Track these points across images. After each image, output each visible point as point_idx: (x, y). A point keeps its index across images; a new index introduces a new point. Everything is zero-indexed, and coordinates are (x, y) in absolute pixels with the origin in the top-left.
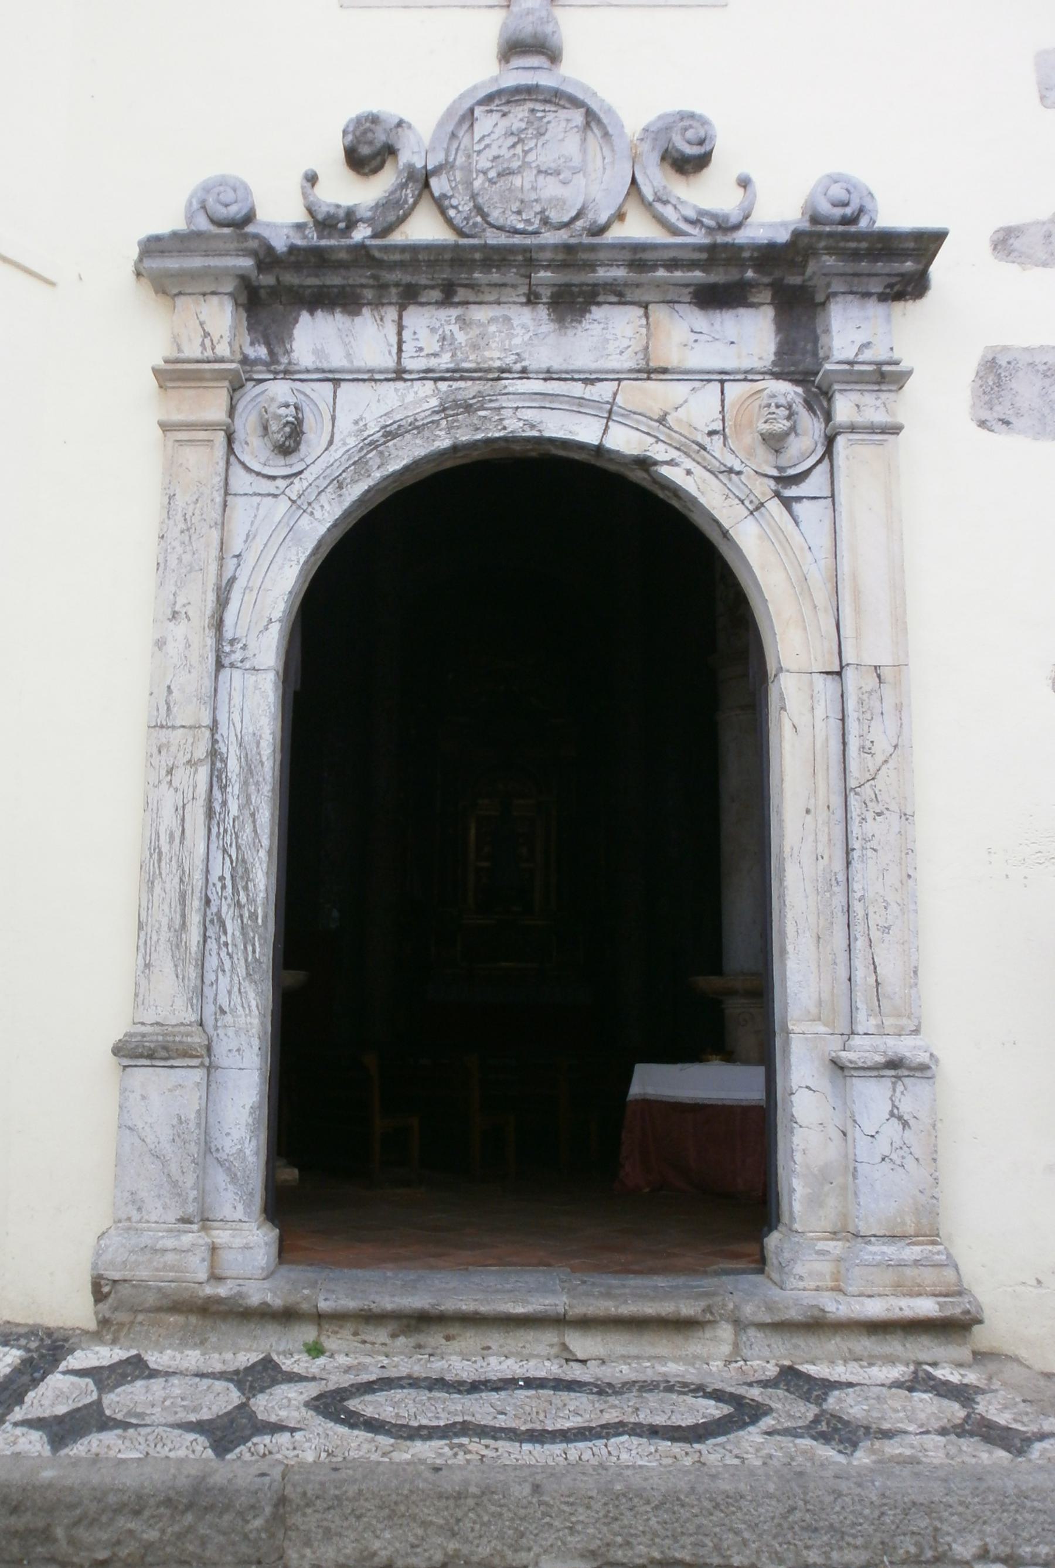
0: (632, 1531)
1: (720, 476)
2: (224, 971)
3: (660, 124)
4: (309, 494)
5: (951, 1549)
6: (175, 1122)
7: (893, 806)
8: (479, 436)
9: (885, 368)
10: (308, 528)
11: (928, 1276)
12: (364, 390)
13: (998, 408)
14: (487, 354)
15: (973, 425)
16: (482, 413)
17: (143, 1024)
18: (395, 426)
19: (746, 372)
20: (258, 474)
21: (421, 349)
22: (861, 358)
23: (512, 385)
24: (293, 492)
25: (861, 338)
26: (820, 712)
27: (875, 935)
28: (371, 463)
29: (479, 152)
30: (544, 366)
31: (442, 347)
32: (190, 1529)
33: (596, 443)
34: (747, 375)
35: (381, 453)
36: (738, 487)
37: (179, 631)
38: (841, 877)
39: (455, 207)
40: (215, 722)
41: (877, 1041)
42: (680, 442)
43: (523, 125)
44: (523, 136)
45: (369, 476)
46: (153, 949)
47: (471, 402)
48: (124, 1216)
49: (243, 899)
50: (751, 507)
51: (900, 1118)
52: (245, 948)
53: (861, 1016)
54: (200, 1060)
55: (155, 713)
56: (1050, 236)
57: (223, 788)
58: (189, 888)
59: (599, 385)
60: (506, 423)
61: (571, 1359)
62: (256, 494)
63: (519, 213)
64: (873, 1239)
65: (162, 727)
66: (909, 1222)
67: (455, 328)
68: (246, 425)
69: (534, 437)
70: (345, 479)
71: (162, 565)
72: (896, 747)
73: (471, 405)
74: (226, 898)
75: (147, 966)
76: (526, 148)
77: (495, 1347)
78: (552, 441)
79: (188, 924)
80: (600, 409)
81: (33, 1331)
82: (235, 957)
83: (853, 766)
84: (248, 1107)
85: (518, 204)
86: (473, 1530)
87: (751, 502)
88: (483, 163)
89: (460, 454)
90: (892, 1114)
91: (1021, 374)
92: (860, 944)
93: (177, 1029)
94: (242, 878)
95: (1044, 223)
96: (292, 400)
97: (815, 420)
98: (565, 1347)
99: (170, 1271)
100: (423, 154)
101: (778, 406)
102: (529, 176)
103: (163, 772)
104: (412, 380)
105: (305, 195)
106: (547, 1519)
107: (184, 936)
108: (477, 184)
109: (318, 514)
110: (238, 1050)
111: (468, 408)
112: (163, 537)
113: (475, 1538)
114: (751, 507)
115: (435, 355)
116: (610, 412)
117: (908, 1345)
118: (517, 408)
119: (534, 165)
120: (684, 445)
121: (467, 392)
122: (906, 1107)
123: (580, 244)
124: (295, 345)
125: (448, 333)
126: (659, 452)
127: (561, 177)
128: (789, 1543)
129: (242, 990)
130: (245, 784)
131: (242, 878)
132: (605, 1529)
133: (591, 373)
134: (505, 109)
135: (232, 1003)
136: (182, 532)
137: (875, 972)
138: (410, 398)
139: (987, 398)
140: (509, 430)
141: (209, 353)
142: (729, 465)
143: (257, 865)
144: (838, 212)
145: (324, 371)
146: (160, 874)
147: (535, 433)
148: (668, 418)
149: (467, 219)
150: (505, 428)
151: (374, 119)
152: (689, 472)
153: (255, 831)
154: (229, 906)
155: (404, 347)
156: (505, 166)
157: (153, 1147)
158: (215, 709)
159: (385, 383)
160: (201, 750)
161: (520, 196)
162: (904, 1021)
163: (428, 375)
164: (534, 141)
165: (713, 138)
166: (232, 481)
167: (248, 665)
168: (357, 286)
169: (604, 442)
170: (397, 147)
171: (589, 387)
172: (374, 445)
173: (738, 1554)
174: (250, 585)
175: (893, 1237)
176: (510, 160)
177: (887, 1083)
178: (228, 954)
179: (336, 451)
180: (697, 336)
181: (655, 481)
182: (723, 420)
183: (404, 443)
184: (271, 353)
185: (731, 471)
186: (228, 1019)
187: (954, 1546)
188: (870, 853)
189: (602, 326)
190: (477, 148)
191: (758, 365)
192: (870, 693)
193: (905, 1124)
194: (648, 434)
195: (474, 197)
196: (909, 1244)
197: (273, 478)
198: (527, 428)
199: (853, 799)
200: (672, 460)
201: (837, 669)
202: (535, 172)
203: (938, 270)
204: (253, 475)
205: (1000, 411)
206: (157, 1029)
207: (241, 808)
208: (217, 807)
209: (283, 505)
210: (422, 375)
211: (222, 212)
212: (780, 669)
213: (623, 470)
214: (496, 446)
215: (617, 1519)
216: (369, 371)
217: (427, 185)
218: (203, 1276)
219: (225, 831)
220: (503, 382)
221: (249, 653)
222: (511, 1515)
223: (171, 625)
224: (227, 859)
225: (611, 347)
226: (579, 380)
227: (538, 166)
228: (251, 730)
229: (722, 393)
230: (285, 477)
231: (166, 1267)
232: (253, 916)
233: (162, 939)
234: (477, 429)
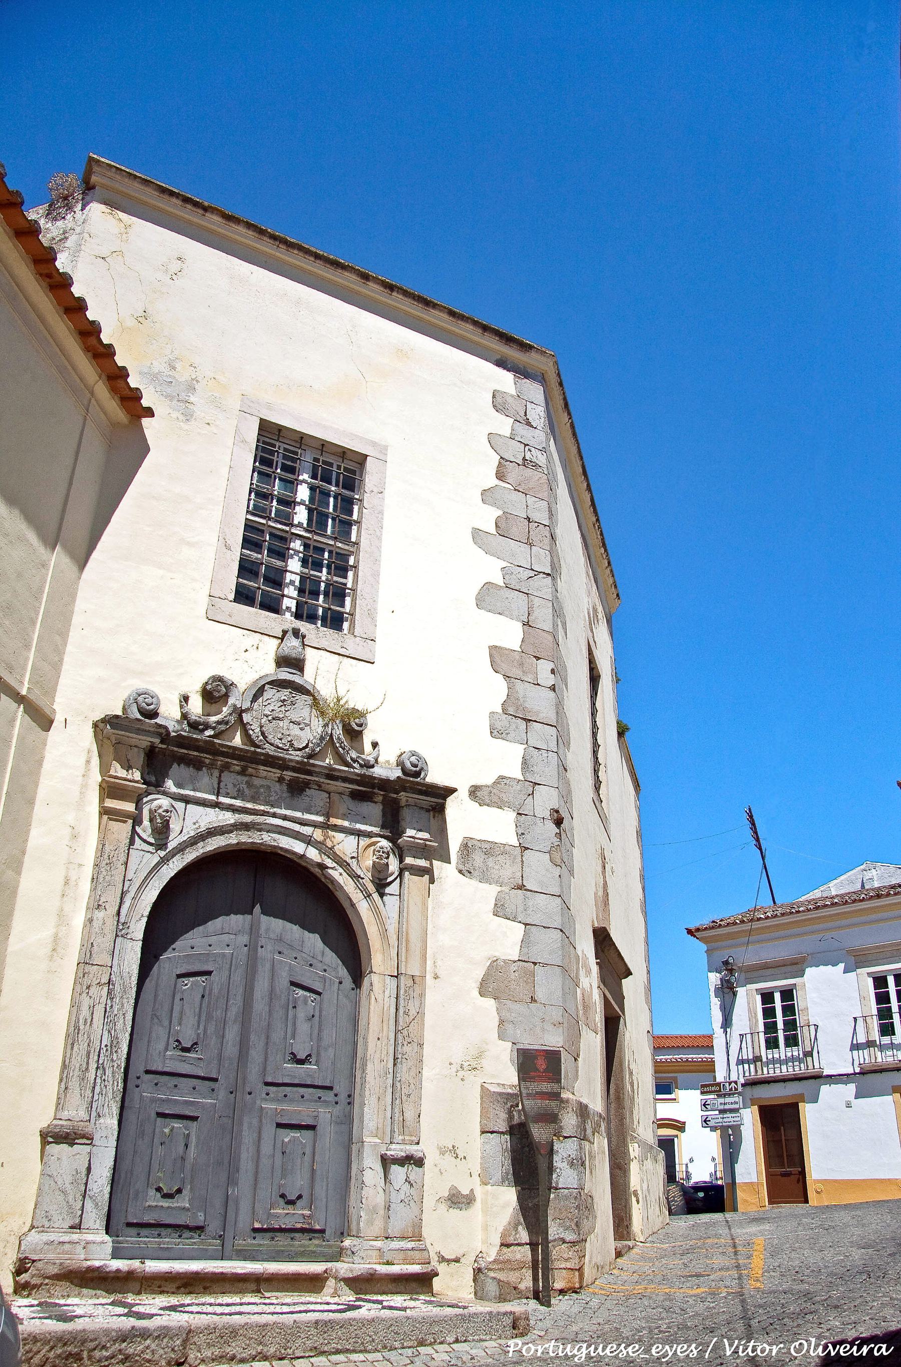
6: (74, 1173)
8: (250, 840)
12: (200, 809)
13: (466, 865)
21: (228, 794)
26: (387, 993)
32: (148, 1347)
38: (391, 1071)
39: (253, 730)
41: (402, 1147)
49: (115, 1058)
51: (410, 1182)
52: (113, 1083)
53: (396, 1135)
63: (281, 739)
78: (281, 848)
83: (401, 1020)
84: (108, 1167)
90: (406, 1180)
102: (286, 722)
105: (181, 707)
106: (299, 1334)
122: (411, 1178)
136: (107, 864)
138: (221, 817)
146: (78, 1040)
150: (262, 839)
152: (341, 874)
161: (282, 732)
162: (413, 1138)
165: (366, 725)
175: (403, 1238)
180: (350, 812)
185: (359, 877)
188: (404, 1060)
198: (272, 841)
199: (400, 1036)
206: (69, 1123)
212: (371, 972)
213: (309, 866)
221: (130, 931)
223: (96, 912)
228: (127, 970)
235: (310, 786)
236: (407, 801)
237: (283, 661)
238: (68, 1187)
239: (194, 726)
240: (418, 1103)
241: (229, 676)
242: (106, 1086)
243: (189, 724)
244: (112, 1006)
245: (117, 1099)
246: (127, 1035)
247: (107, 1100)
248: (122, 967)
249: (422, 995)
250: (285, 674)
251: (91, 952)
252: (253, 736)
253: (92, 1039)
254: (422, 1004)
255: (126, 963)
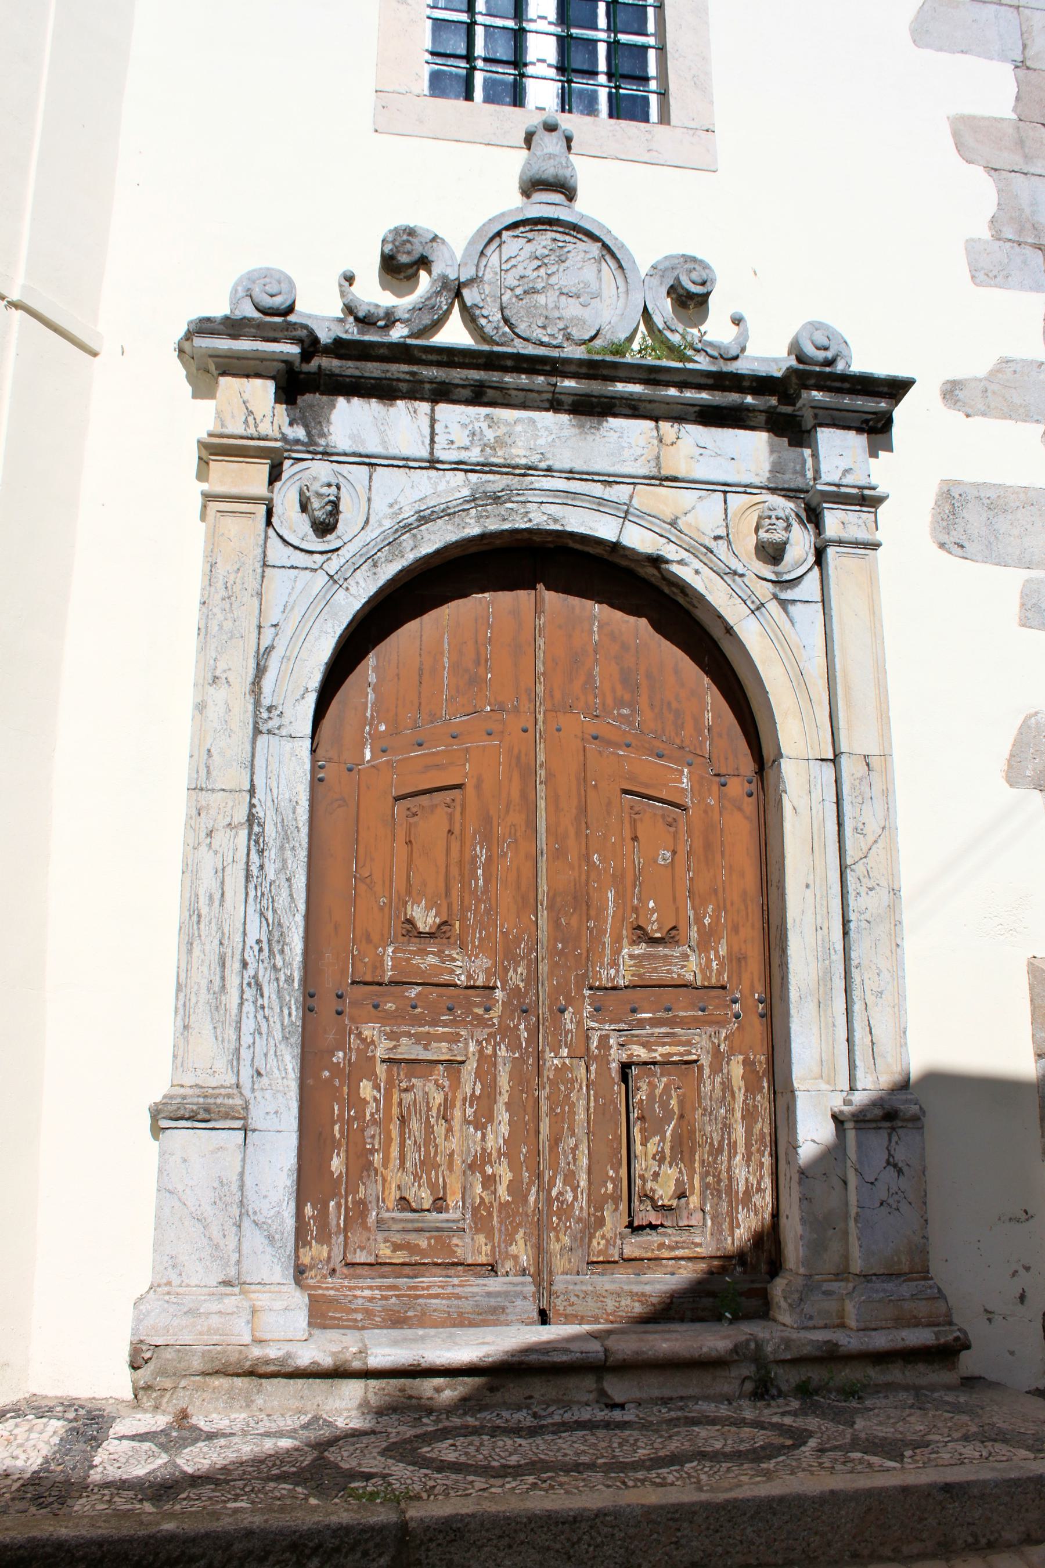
0: (731, 1541)
1: (725, 577)
2: (260, 1033)
3: (667, 264)
4: (346, 571)
5: (1000, 1536)
6: (216, 1184)
7: (884, 883)
8: (506, 526)
9: (867, 492)
10: (343, 603)
11: (922, 1309)
13: (953, 533)
14: (514, 451)
15: (935, 547)
16: (509, 505)
17: (182, 1086)
18: (429, 511)
19: (746, 486)
20: (296, 548)
21: (452, 442)
22: (844, 481)
23: (539, 482)
24: (333, 566)
25: (844, 464)
26: (816, 795)
27: (870, 999)
28: (404, 544)
29: (507, 271)
30: (567, 466)
31: (471, 442)
33: (614, 540)
34: (746, 488)
35: (414, 536)
36: (740, 587)
37: (218, 695)
38: (839, 946)
40: (253, 786)
42: (689, 544)
43: (546, 252)
44: (546, 261)
45: (403, 556)
46: (192, 1011)
47: (500, 494)
48: (164, 1281)
49: (279, 963)
50: (753, 607)
51: (895, 1166)
52: (282, 1011)
54: (242, 1122)
55: (196, 776)
56: (986, 391)
57: (261, 852)
58: (229, 951)
59: (616, 487)
60: (531, 516)
61: (614, 1406)
62: (292, 567)
63: (544, 327)
64: (874, 1278)
65: (202, 789)
66: (904, 1260)
67: (484, 426)
68: (286, 499)
69: (557, 531)
70: (379, 558)
71: (203, 631)
72: (884, 828)
73: (499, 497)
74: (263, 961)
75: (186, 1027)
76: (549, 272)
77: (537, 1395)
78: (572, 535)
79: (228, 986)
80: (618, 509)
81: (70, 1403)
82: (271, 1020)
84: (286, 1169)
85: (543, 319)
86: (587, 1552)
87: (753, 602)
88: (511, 280)
89: (485, 542)
90: (888, 1163)
91: (970, 505)
92: (858, 1007)
93: (217, 1091)
94: (278, 942)
95: (981, 380)
96: (334, 481)
97: (806, 532)
98: (602, 1393)
99: (215, 1334)
100: (456, 268)
101: (778, 519)
103: (203, 835)
104: (444, 470)
105: (343, 294)
107: (223, 998)
108: (505, 298)
109: (353, 590)
110: (276, 1112)
111: (496, 499)
112: (204, 603)
113: (589, 1559)
114: (753, 607)
115: (466, 449)
116: (627, 512)
117: (907, 1373)
118: (542, 503)
119: (556, 287)
120: (693, 547)
121: (496, 485)
122: (900, 1155)
123: (603, 361)
124: (332, 429)
125: (477, 429)
126: (670, 552)
127: (581, 300)
128: (866, 1541)
129: (278, 1053)
130: (282, 848)
131: (278, 942)
132: (707, 1541)
133: (609, 475)
134: (530, 235)
135: (268, 1066)
137: (871, 1033)
138: (442, 486)
139: (945, 524)
140: (535, 522)
141: (252, 431)
142: (733, 568)
143: (294, 929)
144: (821, 355)
145: (361, 456)
146: (200, 936)
147: (558, 527)
148: (679, 522)
149: (497, 328)
150: (530, 520)
151: (411, 232)
152: (697, 572)
153: (291, 895)
154: (266, 969)
155: (437, 439)
156: (531, 285)
157: (193, 1209)
158: (252, 774)
159: (418, 470)
160: (241, 815)
161: (545, 313)
163: (458, 466)
164: (556, 266)
165: (713, 281)
166: (269, 553)
167: (284, 732)
168: (393, 380)
169: (621, 540)
170: (430, 258)
171: (608, 489)
172: (408, 528)
173: (823, 1554)
174: (288, 654)
176: (533, 281)
177: (884, 1134)
178: (265, 1017)
179: (372, 531)
180: (702, 451)
181: (664, 578)
182: (727, 526)
183: (436, 528)
184: (309, 434)
185: (735, 573)
186: (265, 1080)
187: (1003, 1533)
189: (617, 434)
190: (504, 267)
191: (756, 481)
192: (861, 779)
193: (900, 1172)
194: (661, 536)
195: (502, 309)
196: (904, 1281)
197: (311, 552)
198: (550, 522)
199: (850, 877)
200: (682, 560)
201: (832, 757)
202: (557, 293)
203: (902, 413)
204: (291, 548)
205: (957, 535)
206: (198, 1091)
207: (277, 872)
208: (255, 870)
209: (321, 579)
210: (454, 466)
211: (268, 302)
213: (633, 565)
214: (519, 537)
215: (717, 1531)
216: (404, 459)
217: (458, 294)
218: (247, 1339)
219: (263, 894)
220: (530, 478)
221: (285, 721)
222: (622, 1535)
223: (211, 690)
224: (264, 922)
225: (626, 454)
226: (599, 481)
227: (560, 288)
228: (287, 796)
229: (725, 503)
230: (322, 553)
231: (210, 1331)
232: (289, 980)
233: (201, 1001)
234: (504, 520)
235: (617, 410)
236: (816, 416)
237: (532, 186)
238: (208, 1210)
239: (365, 321)
240: (899, 1007)
241: (424, 221)
242: (266, 1018)
243: (357, 319)
244: (262, 867)
245: (292, 1040)
246: (300, 919)
247: (272, 1043)
248: (275, 791)
249: (887, 793)
250: (543, 206)
251: (208, 767)
252: (489, 329)
253: (226, 931)
254: (889, 810)
255: (283, 782)
